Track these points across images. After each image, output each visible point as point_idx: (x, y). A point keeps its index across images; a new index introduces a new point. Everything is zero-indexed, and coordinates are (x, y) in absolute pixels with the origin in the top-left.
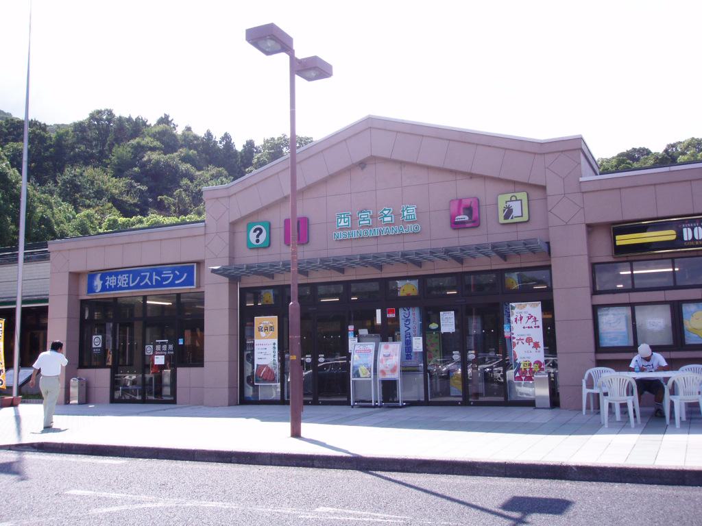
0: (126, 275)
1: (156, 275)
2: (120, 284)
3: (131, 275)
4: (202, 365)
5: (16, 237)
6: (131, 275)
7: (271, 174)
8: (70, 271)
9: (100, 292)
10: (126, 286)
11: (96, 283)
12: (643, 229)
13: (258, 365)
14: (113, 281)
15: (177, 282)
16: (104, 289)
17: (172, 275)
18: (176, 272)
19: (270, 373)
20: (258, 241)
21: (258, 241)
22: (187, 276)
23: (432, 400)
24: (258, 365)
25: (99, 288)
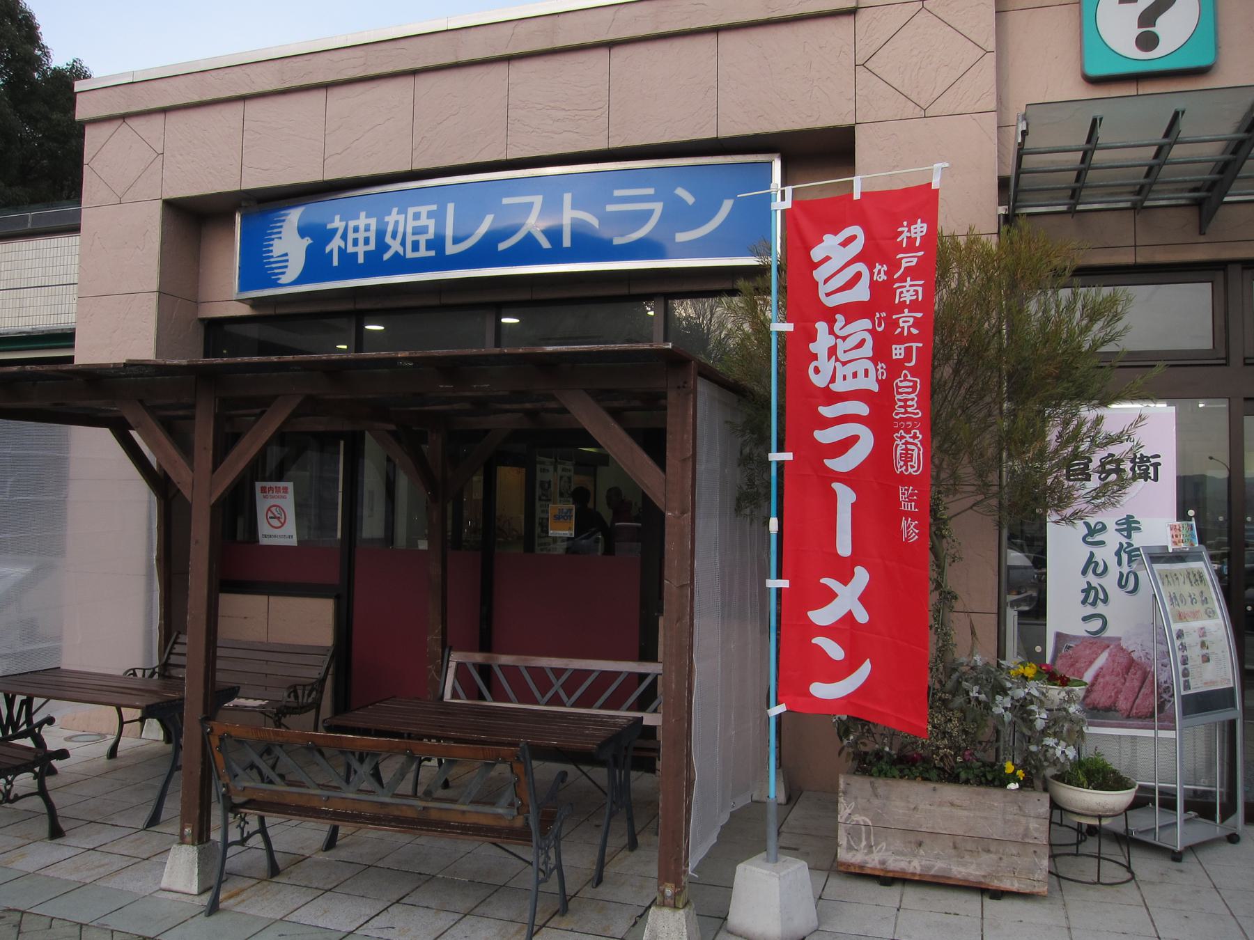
0: (424, 210)
1: (575, 206)
2: (395, 246)
3: (451, 208)
4: (845, 584)
5: (649, 744)
6: (451, 208)
7: (465, 845)
8: (165, 197)
9: (297, 282)
10: (423, 253)
11: (278, 248)
12: (778, 635)
13: (1059, 637)
14: (361, 236)
15: (681, 237)
16: (316, 264)
17: (658, 207)
18: (681, 192)
19: (1133, 681)
20: (1147, 41)
21: (1147, 41)
22: (637, 527)
23: (452, 665)
24: (1059, 637)
25: (296, 266)
